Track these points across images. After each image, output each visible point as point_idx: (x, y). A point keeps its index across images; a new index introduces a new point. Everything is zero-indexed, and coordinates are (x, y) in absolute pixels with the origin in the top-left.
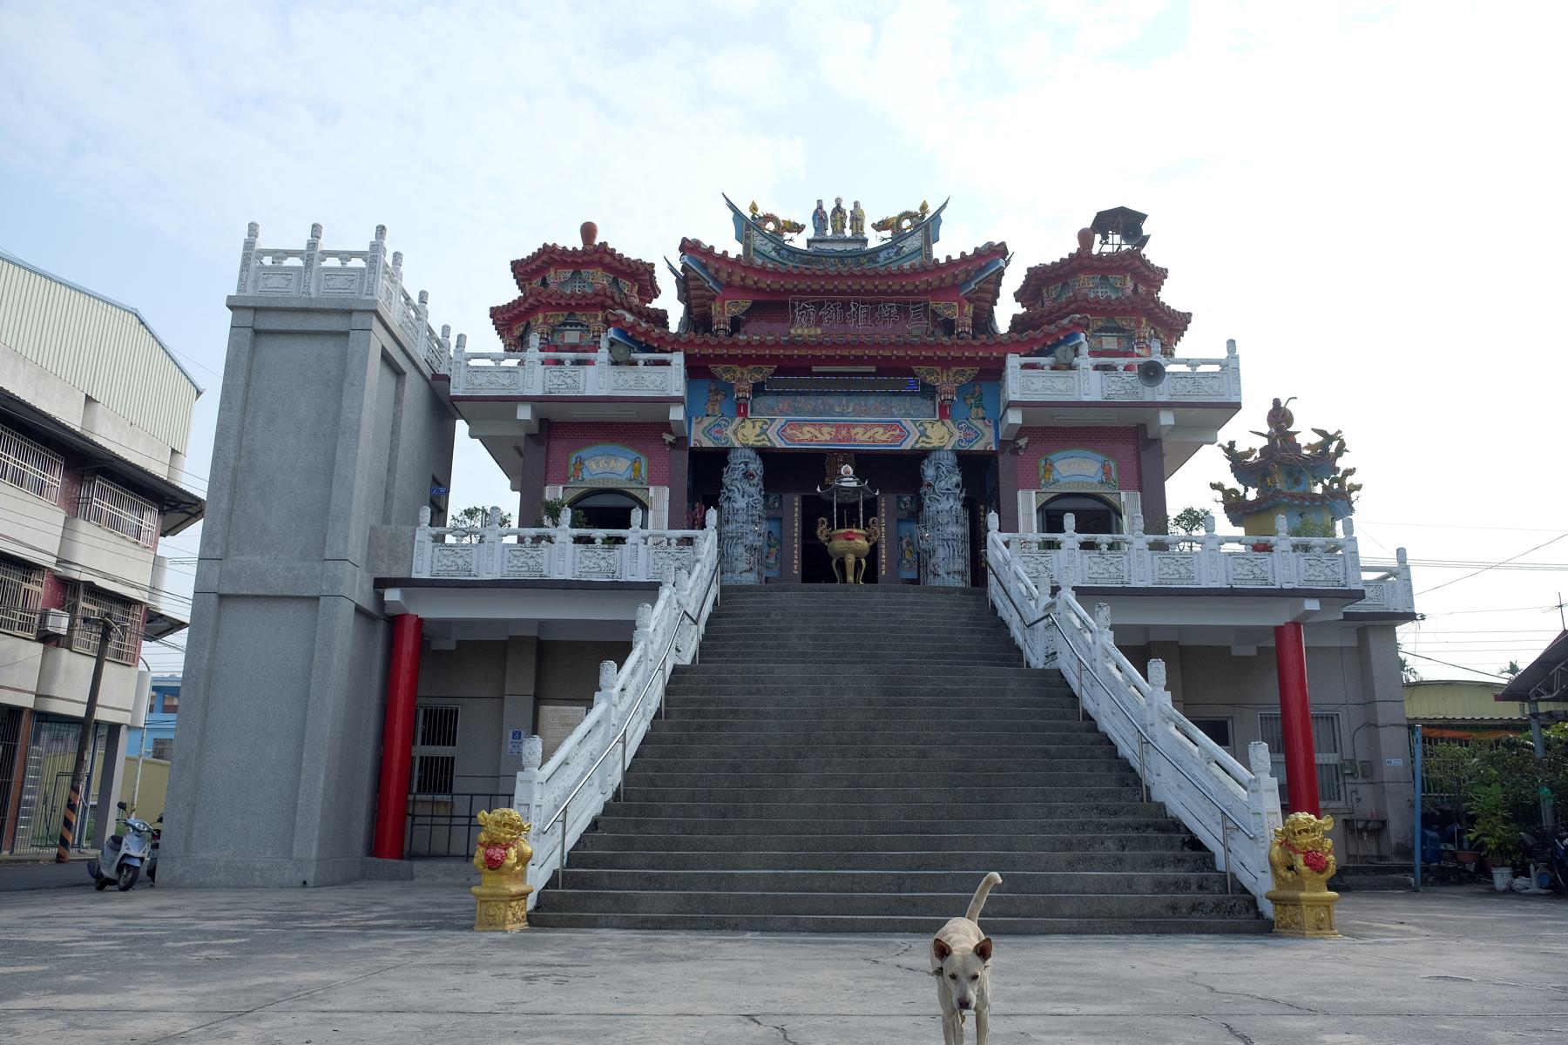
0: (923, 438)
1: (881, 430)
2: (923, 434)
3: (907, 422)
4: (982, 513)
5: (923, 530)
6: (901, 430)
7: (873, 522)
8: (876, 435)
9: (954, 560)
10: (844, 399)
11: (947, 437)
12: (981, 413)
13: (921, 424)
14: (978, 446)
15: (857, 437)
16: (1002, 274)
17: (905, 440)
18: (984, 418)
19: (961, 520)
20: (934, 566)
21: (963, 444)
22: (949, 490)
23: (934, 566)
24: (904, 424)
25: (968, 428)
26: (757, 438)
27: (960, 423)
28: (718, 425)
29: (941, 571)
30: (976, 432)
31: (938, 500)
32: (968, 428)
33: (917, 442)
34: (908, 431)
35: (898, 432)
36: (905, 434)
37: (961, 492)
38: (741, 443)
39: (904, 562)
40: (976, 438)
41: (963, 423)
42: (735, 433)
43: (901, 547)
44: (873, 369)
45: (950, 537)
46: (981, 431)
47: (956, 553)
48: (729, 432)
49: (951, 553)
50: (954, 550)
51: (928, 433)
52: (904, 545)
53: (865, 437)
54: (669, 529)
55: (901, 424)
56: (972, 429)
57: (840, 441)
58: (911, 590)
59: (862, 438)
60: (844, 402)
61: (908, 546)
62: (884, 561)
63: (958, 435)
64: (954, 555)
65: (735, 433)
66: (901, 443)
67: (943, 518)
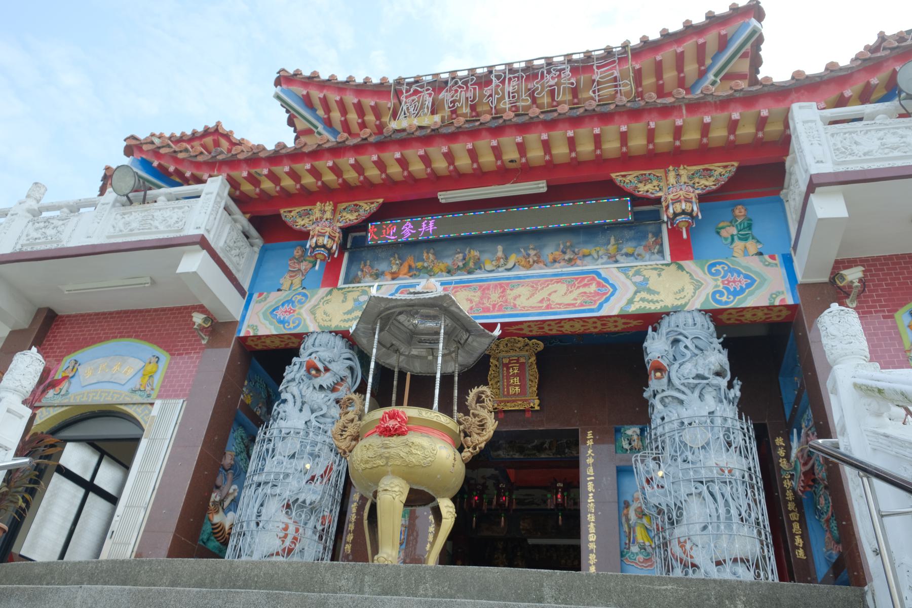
0: (643, 295)
1: (562, 288)
2: (642, 287)
3: (610, 271)
4: (781, 452)
5: (652, 464)
6: (599, 284)
7: (479, 400)
8: (552, 297)
9: (729, 526)
10: (500, 248)
11: (689, 289)
12: (752, 247)
13: (638, 273)
14: (756, 299)
15: (518, 302)
16: (760, 40)
17: (607, 300)
18: (760, 254)
19: (738, 439)
20: (682, 545)
21: (724, 299)
22: (703, 377)
23: (682, 545)
24: (604, 275)
25: (731, 271)
26: (346, 317)
27: (713, 265)
28: (288, 302)
29: (701, 557)
30: (747, 277)
31: (681, 402)
32: (731, 271)
33: (631, 302)
34: (613, 286)
35: (593, 288)
36: (607, 289)
37: (730, 386)
38: (320, 326)
39: (635, 549)
40: (748, 286)
41: (720, 263)
42: (313, 312)
43: (628, 520)
44: (540, 186)
45: (715, 474)
46: (756, 273)
47: (734, 512)
48: (304, 312)
49: (722, 511)
50: (727, 503)
51: (651, 285)
52: (633, 516)
53: (534, 301)
54: (578, 568)
55: (599, 275)
56: (739, 273)
57: (486, 310)
58: (547, 591)
59: (527, 303)
60: (500, 254)
61: (640, 518)
62: (592, 546)
63: (710, 284)
64: (729, 518)
65: (313, 312)
66: (600, 307)
67: (695, 437)
